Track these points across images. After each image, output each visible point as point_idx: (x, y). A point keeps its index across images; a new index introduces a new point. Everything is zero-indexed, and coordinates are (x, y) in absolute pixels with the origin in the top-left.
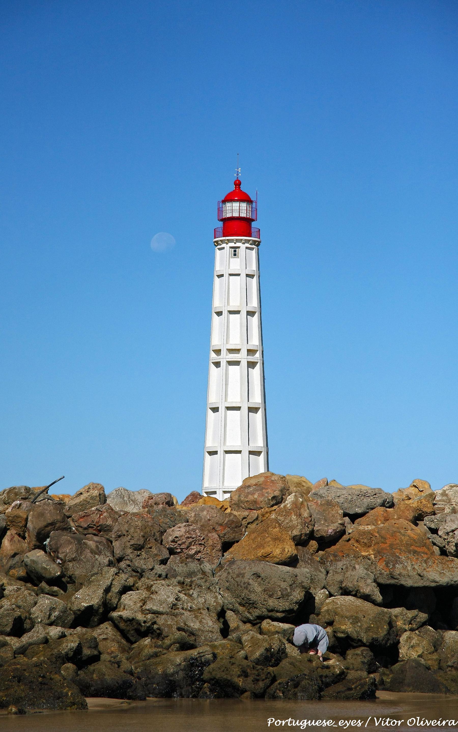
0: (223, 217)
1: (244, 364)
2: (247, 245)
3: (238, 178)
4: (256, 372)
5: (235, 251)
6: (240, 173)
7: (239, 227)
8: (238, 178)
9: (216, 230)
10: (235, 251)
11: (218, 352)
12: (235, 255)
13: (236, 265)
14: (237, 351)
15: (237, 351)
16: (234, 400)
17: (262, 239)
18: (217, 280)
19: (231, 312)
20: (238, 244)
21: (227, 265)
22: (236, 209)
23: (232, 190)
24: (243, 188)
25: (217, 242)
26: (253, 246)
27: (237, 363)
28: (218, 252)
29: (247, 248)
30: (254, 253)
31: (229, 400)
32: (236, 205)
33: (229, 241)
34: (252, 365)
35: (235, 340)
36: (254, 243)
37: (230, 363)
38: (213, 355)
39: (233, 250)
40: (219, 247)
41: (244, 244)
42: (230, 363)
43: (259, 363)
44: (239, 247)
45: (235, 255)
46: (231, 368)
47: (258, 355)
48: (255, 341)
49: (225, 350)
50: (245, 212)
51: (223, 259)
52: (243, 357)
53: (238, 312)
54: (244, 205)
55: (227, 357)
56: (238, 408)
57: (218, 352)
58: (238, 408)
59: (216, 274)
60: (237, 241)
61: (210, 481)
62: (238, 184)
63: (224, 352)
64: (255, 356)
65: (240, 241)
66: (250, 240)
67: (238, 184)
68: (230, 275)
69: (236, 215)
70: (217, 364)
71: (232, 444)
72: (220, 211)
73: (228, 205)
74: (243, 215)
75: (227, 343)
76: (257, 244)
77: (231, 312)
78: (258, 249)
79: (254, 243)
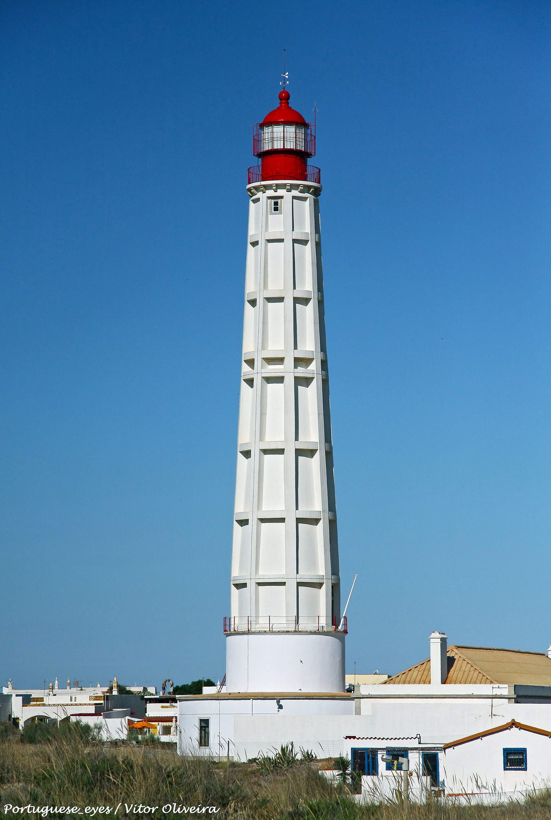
0: (262, 150)
1: (290, 381)
2: (295, 193)
3: (284, 88)
4: (311, 395)
5: (276, 204)
6: (288, 79)
7: (288, 165)
8: (284, 88)
9: (251, 170)
10: (276, 204)
11: (251, 363)
12: (276, 209)
13: (278, 225)
14: (280, 360)
15: (280, 360)
16: (273, 439)
17: (324, 183)
18: (248, 306)
19: (270, 300)
20: (280, 192)
21: (264, 225)
22: (281, 137)
23: (275, 108)
24: (293, 104)
25: (249, 190)
26: (306, 195)
27: (280, 380)
28: (252, 205)
29: (294, 198)
30: (307, 207)
31: (267, 438)
32: (278, 130)
33: (267, 187)
34: (302, 381)
35: (278, 344)
36: (307, 189)
37: (269, 380)
38: (245, 368)
39: (273, 201)
40: (254, 197)
41: (289, 191)
42: (269, 380)
43: (315, 380)
44: (282, 197)
45: (276, 209)
46: (271, 387)
47: (314, 367)
48: (309, 344)
49: (260, 360)
50: (294, 140)
51: (261, 219)
52: (287, 370)
53: (280, 299)
54: (291, 130)
55: (263, 371)
56: (281, 451)
57: (251, 363)
58: (281, 451)
59: (249, 240)
60: (278, 187)
61: (241, 568)
62: (285, 97)
63: (258, 363)
64: (309, 368)
65: (283, 186)
66: (298, 186)
67: (285, 97)
68: (269, 241)
69: (278, 145)
70: (250, 382)
71: (270, 508)
72: (257, 141)
73: (267, 130)
74: (290, 145)
75: (263, 348)
76: (317, 192)
77: (270, 300)
78: (316, 202)
79: (307, 189)
